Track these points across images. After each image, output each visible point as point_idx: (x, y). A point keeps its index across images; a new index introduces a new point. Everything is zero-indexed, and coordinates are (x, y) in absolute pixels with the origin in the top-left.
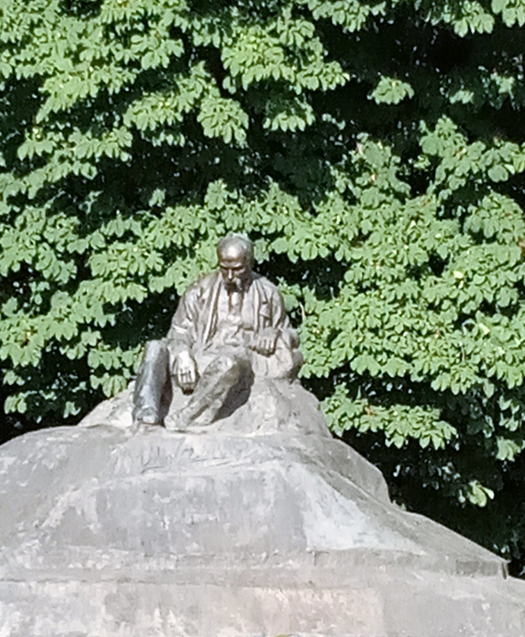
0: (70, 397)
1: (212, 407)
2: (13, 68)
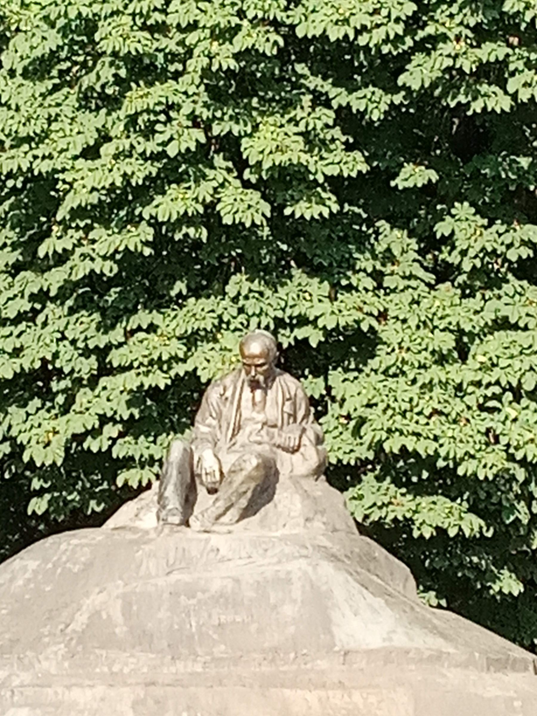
0: (93, 496)
1: (237, 506)
2: (31, 163)
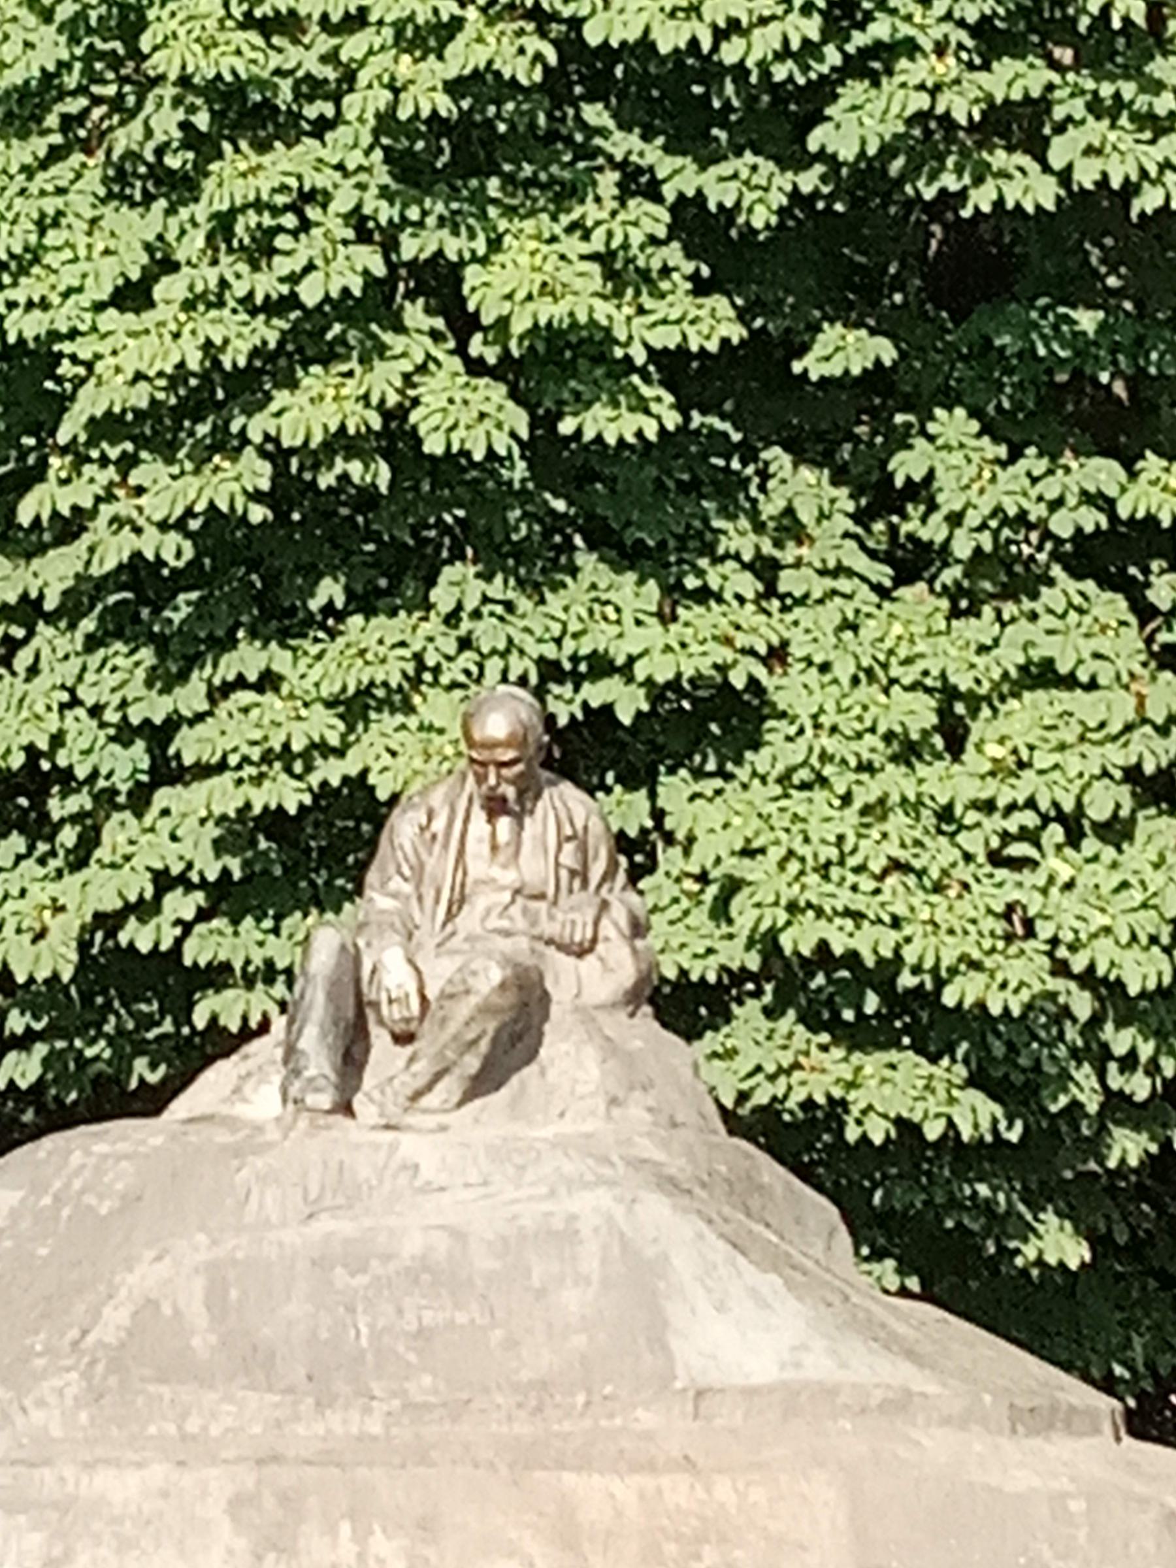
0: (141, 1048)
1: (457, 1071)
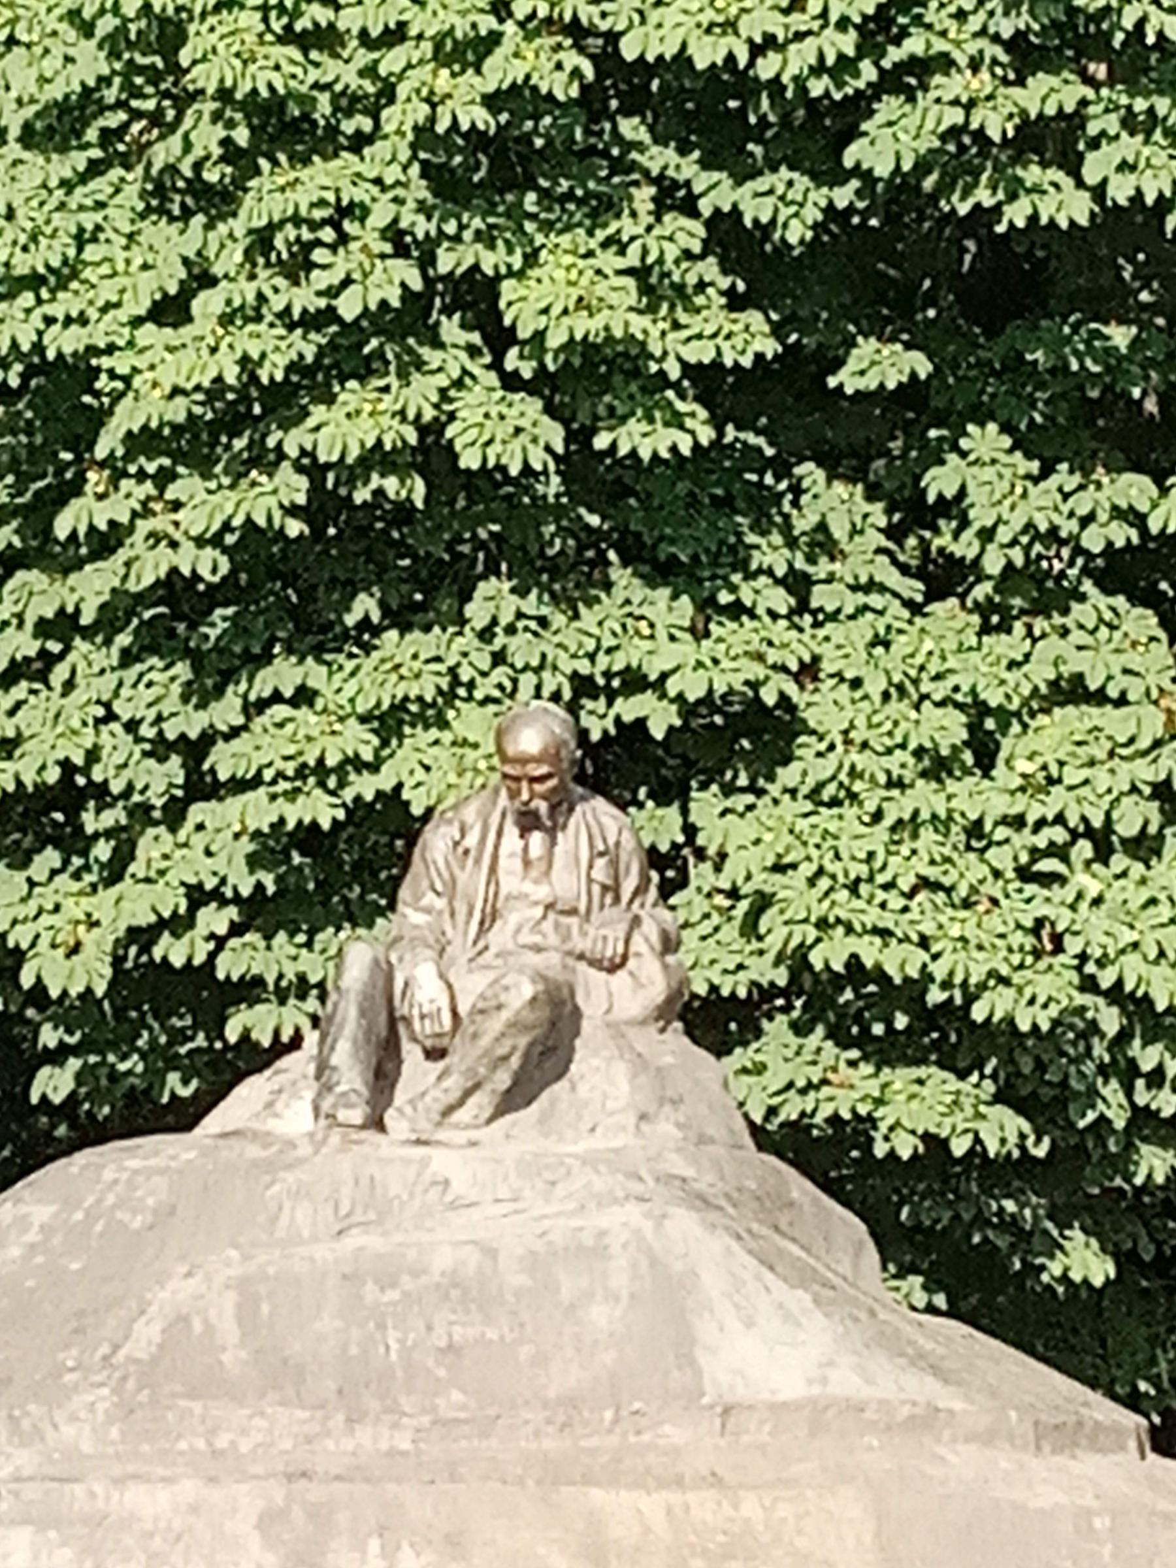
0: (173, 1062)
1: (488, 1087)
2: (40, 334)
